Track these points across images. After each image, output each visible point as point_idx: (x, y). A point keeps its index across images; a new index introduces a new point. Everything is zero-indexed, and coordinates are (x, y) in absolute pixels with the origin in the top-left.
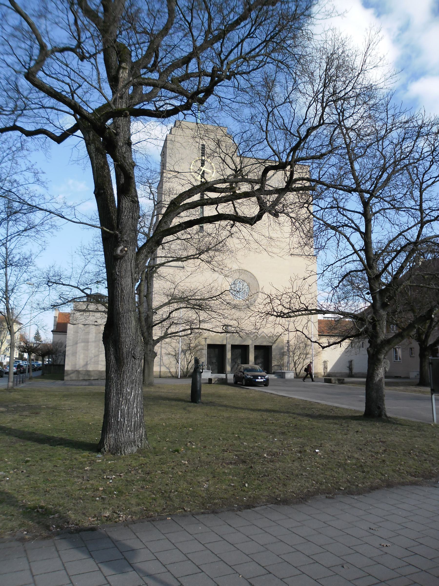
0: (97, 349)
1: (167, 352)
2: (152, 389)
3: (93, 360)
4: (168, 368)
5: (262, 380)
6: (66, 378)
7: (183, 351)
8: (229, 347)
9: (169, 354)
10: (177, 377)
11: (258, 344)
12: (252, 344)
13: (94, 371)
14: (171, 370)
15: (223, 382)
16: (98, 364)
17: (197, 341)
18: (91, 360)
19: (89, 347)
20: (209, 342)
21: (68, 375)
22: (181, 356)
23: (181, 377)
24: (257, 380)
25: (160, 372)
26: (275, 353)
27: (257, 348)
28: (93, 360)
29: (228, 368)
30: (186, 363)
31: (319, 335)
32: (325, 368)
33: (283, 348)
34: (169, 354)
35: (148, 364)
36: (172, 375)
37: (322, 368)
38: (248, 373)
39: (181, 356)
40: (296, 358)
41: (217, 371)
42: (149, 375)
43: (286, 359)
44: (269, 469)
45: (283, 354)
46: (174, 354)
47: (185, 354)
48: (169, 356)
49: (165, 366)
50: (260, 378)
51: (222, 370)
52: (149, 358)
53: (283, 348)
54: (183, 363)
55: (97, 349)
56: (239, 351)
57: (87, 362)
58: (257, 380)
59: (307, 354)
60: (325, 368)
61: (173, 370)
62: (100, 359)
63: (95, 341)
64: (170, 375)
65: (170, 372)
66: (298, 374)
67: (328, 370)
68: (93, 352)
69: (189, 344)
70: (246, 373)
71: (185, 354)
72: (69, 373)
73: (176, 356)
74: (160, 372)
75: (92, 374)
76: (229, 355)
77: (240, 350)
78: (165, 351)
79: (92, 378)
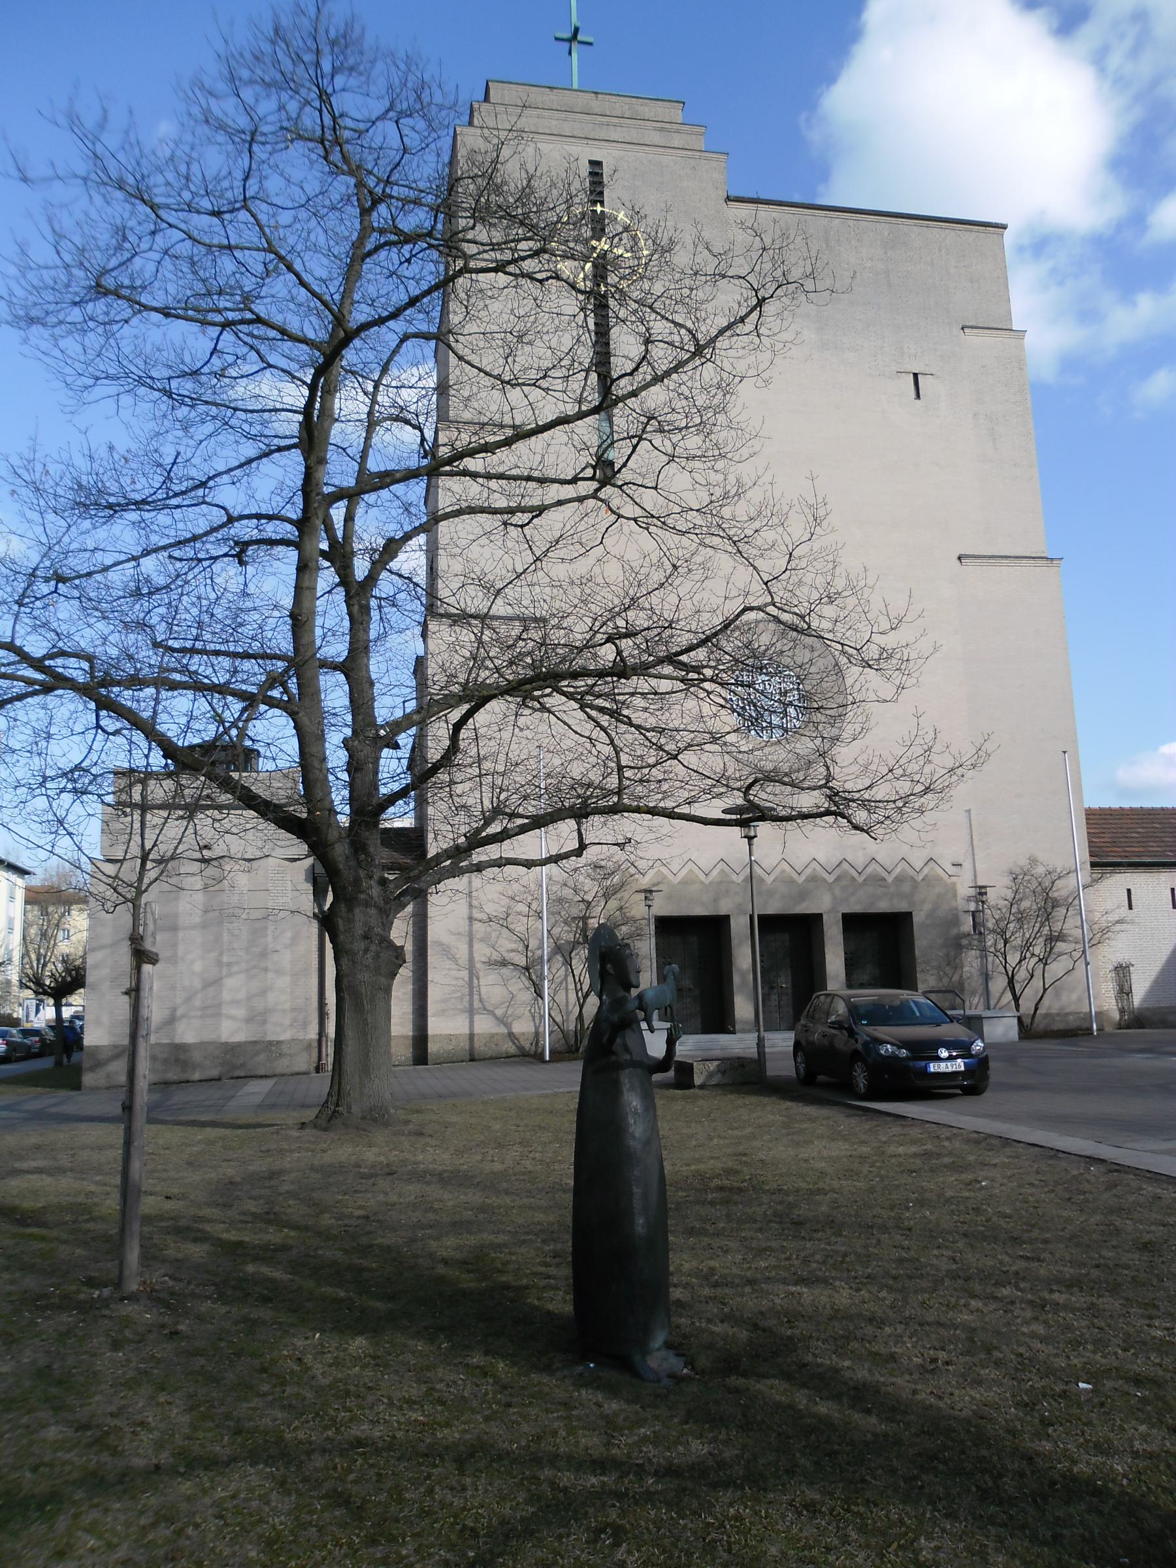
0: (213, 955)
1: (495, 956)
2: (374, 1151)
3: (197, 1002)
4: (501, 1021)
5: (959, 1065)
6: (88, 1079)
7: (557, 949)
8: (739, 927)
9: (504, 963)
10: (538, 1057)
11: (857, 908)
12: (833, 910)
13: (202, 1044)
14: (517, 1028)
15: (745, 1077)
16: (217, 1015)
17: (613, 904)
18: (189, 999)
19: (181, 949)
20: (663, 907)
21: (97, 1065)
22: (553, 971)
23: (557, 1056)
24: (933, 1067)
25: (471, 1036)
26: (924, 941)
27: (853, 923)
28: (197, 1002)
29: (743, 1008)
30: (572, 997)
31: (1093, 865)
32: (1124, 991)
33: (954, 920)
34: (504, 963)
35: (359, 1008)
36: (520, 1048)
37: (1112, 994)
38: (882, 1032)
39: (553, 971)
40: (1013, 959)
41: (697, 1022)
42: (366, 1070)
43: (971, 962)
44: (1025, 1544)
45: (957, 945)
46: (523, 963)
47: (568, 962)
48: (505, 971)
49: (492, 1013)
50: (944, 1053)
51: (718, 1019)
52: (364, 976)
53: (954, 920)
54: (560, 997)
55: (213, 955)
56: (783, 939)
57: (174, 1010)
58: (933, 1067)
59: (1053, 939)
60: (1124, 991)
61: (523, 1027)
62: (226, 996)
63: (204, 926)
64: (512, 1049)
65: (511, 1035)
66: (1027, 1021)
67: (1137, 998)
68: (198, 967)
69: (584, 919)
70: (867, 1031)
71: (568, 962)
72: (103, 1056)
73: (530, 971)
74: (471, 1036)
75: (197, 1056)
76: (743, 957)
77: (786, 936)
78: (488, 951)
79: (197, 1076)
